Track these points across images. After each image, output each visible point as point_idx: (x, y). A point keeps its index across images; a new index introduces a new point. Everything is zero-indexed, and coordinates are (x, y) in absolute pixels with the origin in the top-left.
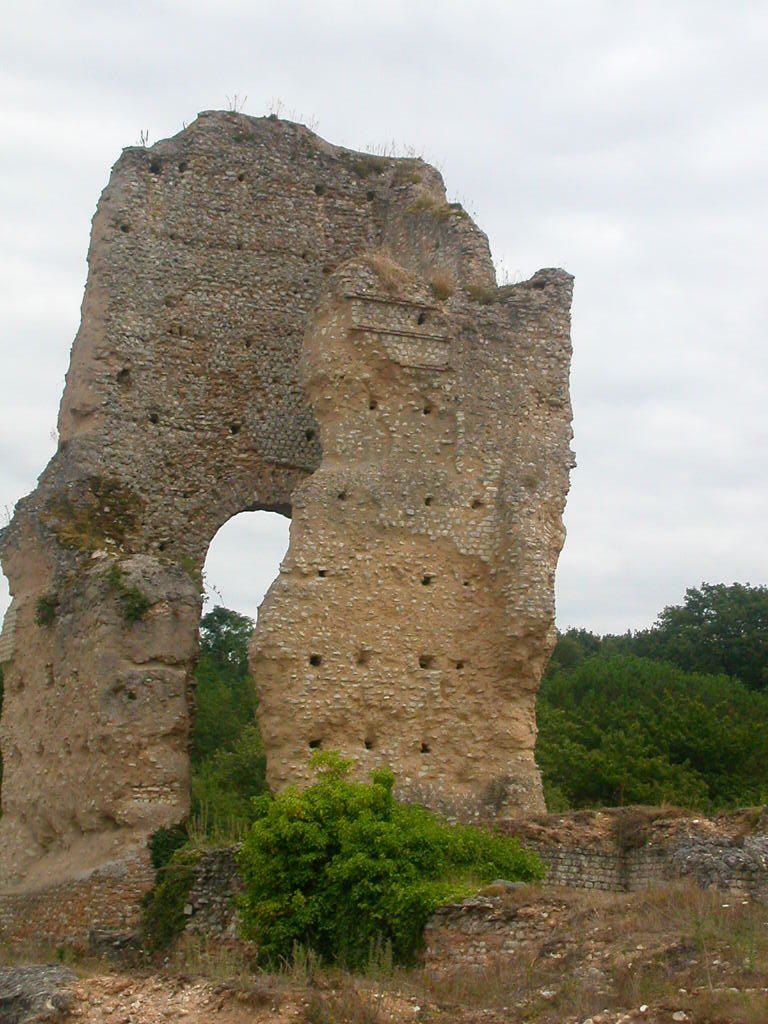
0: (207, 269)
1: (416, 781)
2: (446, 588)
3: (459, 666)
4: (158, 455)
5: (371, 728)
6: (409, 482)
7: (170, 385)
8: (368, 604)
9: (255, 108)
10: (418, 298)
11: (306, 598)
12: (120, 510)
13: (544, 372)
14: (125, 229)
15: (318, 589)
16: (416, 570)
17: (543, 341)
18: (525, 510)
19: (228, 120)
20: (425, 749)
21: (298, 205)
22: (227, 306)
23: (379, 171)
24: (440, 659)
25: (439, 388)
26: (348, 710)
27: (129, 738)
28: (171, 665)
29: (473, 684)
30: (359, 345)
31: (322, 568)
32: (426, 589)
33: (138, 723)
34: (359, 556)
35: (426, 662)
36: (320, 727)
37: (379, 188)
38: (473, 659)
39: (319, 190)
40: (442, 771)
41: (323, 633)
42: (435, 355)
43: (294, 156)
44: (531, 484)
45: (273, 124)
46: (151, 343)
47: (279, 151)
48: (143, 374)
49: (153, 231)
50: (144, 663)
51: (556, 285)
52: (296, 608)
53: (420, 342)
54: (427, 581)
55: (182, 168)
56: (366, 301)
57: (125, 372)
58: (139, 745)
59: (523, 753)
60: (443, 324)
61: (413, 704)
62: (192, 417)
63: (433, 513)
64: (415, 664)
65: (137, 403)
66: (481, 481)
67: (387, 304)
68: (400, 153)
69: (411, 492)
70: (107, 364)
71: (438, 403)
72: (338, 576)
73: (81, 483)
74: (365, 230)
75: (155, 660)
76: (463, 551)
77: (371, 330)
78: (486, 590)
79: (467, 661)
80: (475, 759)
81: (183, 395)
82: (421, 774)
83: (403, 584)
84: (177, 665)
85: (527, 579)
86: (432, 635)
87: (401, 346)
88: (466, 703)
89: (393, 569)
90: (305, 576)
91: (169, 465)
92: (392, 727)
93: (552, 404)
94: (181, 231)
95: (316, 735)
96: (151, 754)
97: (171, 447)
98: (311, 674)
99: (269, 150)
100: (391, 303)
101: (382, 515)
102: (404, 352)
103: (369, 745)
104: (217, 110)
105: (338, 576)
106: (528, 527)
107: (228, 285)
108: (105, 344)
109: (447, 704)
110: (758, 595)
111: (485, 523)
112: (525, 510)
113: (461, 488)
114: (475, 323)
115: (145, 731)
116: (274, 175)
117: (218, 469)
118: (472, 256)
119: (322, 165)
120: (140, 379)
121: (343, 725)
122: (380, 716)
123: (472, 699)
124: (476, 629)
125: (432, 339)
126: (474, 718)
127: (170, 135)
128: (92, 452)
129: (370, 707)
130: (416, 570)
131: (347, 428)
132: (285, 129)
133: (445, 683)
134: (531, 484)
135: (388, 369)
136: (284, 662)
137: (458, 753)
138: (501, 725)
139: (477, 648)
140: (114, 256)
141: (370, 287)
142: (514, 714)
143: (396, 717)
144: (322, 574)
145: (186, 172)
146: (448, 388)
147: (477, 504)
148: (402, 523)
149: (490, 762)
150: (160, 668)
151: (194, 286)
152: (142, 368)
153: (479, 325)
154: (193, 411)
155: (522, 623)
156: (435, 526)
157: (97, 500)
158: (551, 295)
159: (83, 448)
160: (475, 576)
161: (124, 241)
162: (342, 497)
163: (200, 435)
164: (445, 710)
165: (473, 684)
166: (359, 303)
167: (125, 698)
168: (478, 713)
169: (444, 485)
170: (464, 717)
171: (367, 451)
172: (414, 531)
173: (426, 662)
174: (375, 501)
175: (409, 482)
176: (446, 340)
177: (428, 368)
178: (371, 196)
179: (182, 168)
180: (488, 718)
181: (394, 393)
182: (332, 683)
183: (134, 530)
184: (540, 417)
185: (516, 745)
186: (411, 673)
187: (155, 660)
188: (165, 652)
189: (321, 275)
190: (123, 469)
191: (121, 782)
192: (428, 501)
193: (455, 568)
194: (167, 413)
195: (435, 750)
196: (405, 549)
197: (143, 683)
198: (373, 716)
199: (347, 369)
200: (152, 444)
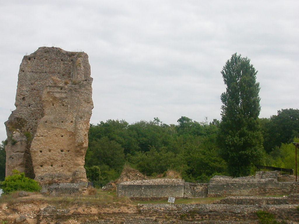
0: (39, 77)
1: (60, 172)
2: (66, 138)
3: (68, 151)
4: (30, 112)
5: (52, 163)
6: (58, 119)
7: (32, 100)
8: (51, 141)
9: (50, 46)
10: (61, 85)
11: (39, 141)
12: (22, 123)
13: (86, 97)
14: (23, 71)
15: (41, 139)
16: (60, 135)
17: (86, 91)
18: (79, 123)
19: (43, 49)
20: (62, 166)
21: (57, 63)
22: (43, 84)
23: (74, 55)
24: (64, 150)
25: (65, 101)
26: (47, 160)
27: (12, 166)
28: (21, 152)
29: (71, 154)
30: (49, 95)
31: (42, 135)
32: (62, 138)
33: (14, 163)
34: (49, 133)
35: (62, 151)
36: (42, 163)
37: (74, 59)
38: (71, 150)
39: (62, 60)
40: (65, 170)
41: (42, 147)
42: (64, 95)
43: (57, 54)
44: (81, 118)
45: (53, 49)
46: (29, 92)
47: (53, 53)
48: (27, 98)
49: (28, 71)
50: (16, 152)
51: (89, 80)
52: (37, 142)
53: (61, 93)
54: (62, 136)
55: (35, 59)
56: (50, 86)
57: (24, 98)
58: (14, 167)
59: (80, 166)
60: (66, 89)
61: (59, 158)
62: (37, 105)
63: (63, 124)
64: (60, 151)
65: (26, 103)
66: (72, 118)
67: (54, 87)
68: (79, 51)
69: (59, 120)
70: (20, 97)
71: (64, 104)
72: (45, 136)
73: (15, 119)
74: (71, 67)
75: (18, 152)
76: (69, 131)
77: (51, 92)
78: (73, 137)
79: (70, 150)
80: (71, 168)
81: (35, 101)
82: (61, 171)
83: (58, 137)
84: (22, 152)
85: (78, 135)
86: (63, 146)
87: (57, 94)
88: (69, 158)
89: (55, 134)
90: (39, 137)
91: (32, 114)
92: (55, 163)
93: (88, 102)
94: (34, 71)
95: (42, 165)
96: (16, 168)
97: (32, 111)
98: (40, 154)
99: (52, 53)
100: (55, 86)
101: (53, 125)
102: (57, 95)
103: (52, 166)
104: (42, 47)
105: (45, 136)
106: (79, 126)
107: (43, 80)
108: (19, 93)
109: (66, 158)
110: (297, 111)
111: (73, 125)
112: (79, 123)
113: (69, 119)
114: (72, 89)
115: (15, 164)
116: (52, 58)
117: (42, 114)
118: (79, 74)
119: (62, 55)
120: (26, 99)
121: (46, 162)
122: (53, 161)
123: (71, 157)
124: (71, 144)
125: (63, 93)
126: (71, 160)
127: (33, 53)
128: (17, 113)
129: (51, 159)
130: (60, 135)
131: (48, 109)
132: (55, 49)
133: (65, 154)
134: (81, 118)
135: (55, 98)
136: (35, 152)
137: (68, 167)
138: (76, 162)
139: (72, 148)
140: (21, 77)
141: (51, 84)
142: (78, 159)
143: (56, 161)
144: (42, 136)
145: (35, 59)
146: (66, 101)
147: (72, 122)
148: (57, 126)
149: (74, 168)
150: (18, 153)
151: (37, 81)
152: (27, 97)
153: (73, 89)
154: (37, 104)
155: (77, 143)
156: (63, 127)
157: (18, 122)
158: (87, 82)
159: (15, 112)
160: (71, 135)
161: (23, 74)
162: (46, 122)
163: (38, 108)
164: (65, 159)
165: (71, 154)
166: (49, 87)
167: (12, 159)
168: (72, 159)
169: (65, 119)
170: (69, 160)
171: (52, 113)
172: (59, 127)
173: (62, 151)
174: (52, 123)
175: (58, 119)
176: (66, 93)
177: (62, 98)
178: (72, 60)
179: (35, 59)
180: (74, 160)
181: (57, 103)
182: (44, 155)
183: (23, 127)
184: (84, 105)
185: (79, 165)
186: (59, 153)
187: (18, 152)
188: (19, 150)
189: (62, 76)
190: (23, 116)
191: (11, 173)
192: (62, 122)
193: (67, 134)
194: (32, 105)
195: (64, 166)
196: (58, 131)
197: (15, 156)
198: (52, 161)
199: (47, 99)
200: (29, 111)
